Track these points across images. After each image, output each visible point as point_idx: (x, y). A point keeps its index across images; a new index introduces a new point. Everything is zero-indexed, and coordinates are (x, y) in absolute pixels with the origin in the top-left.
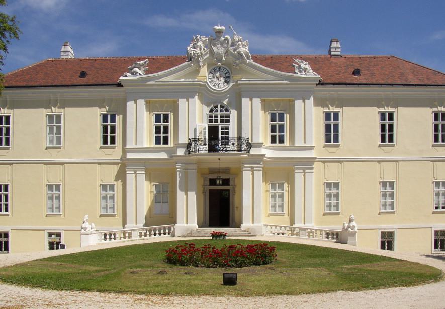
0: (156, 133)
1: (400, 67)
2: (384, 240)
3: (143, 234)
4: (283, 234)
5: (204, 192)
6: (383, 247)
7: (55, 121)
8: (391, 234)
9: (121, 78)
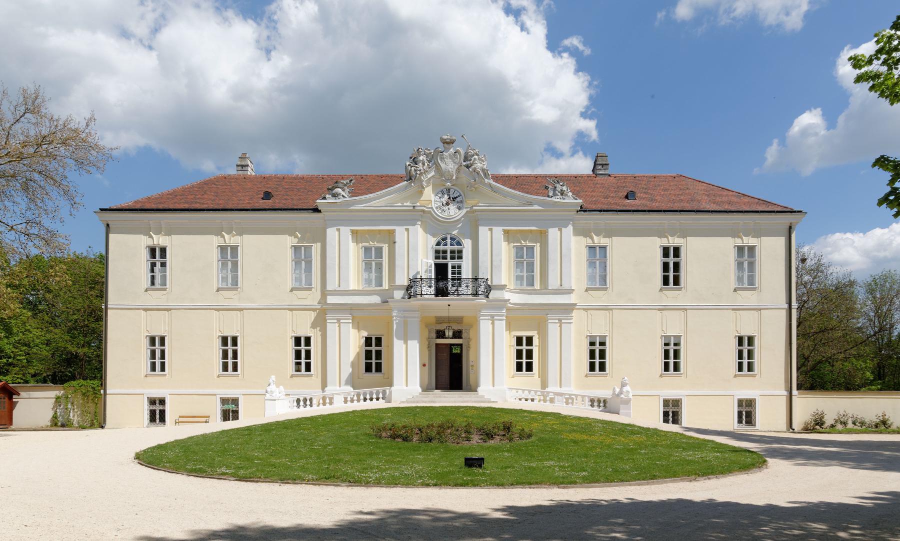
5: (429, 346)
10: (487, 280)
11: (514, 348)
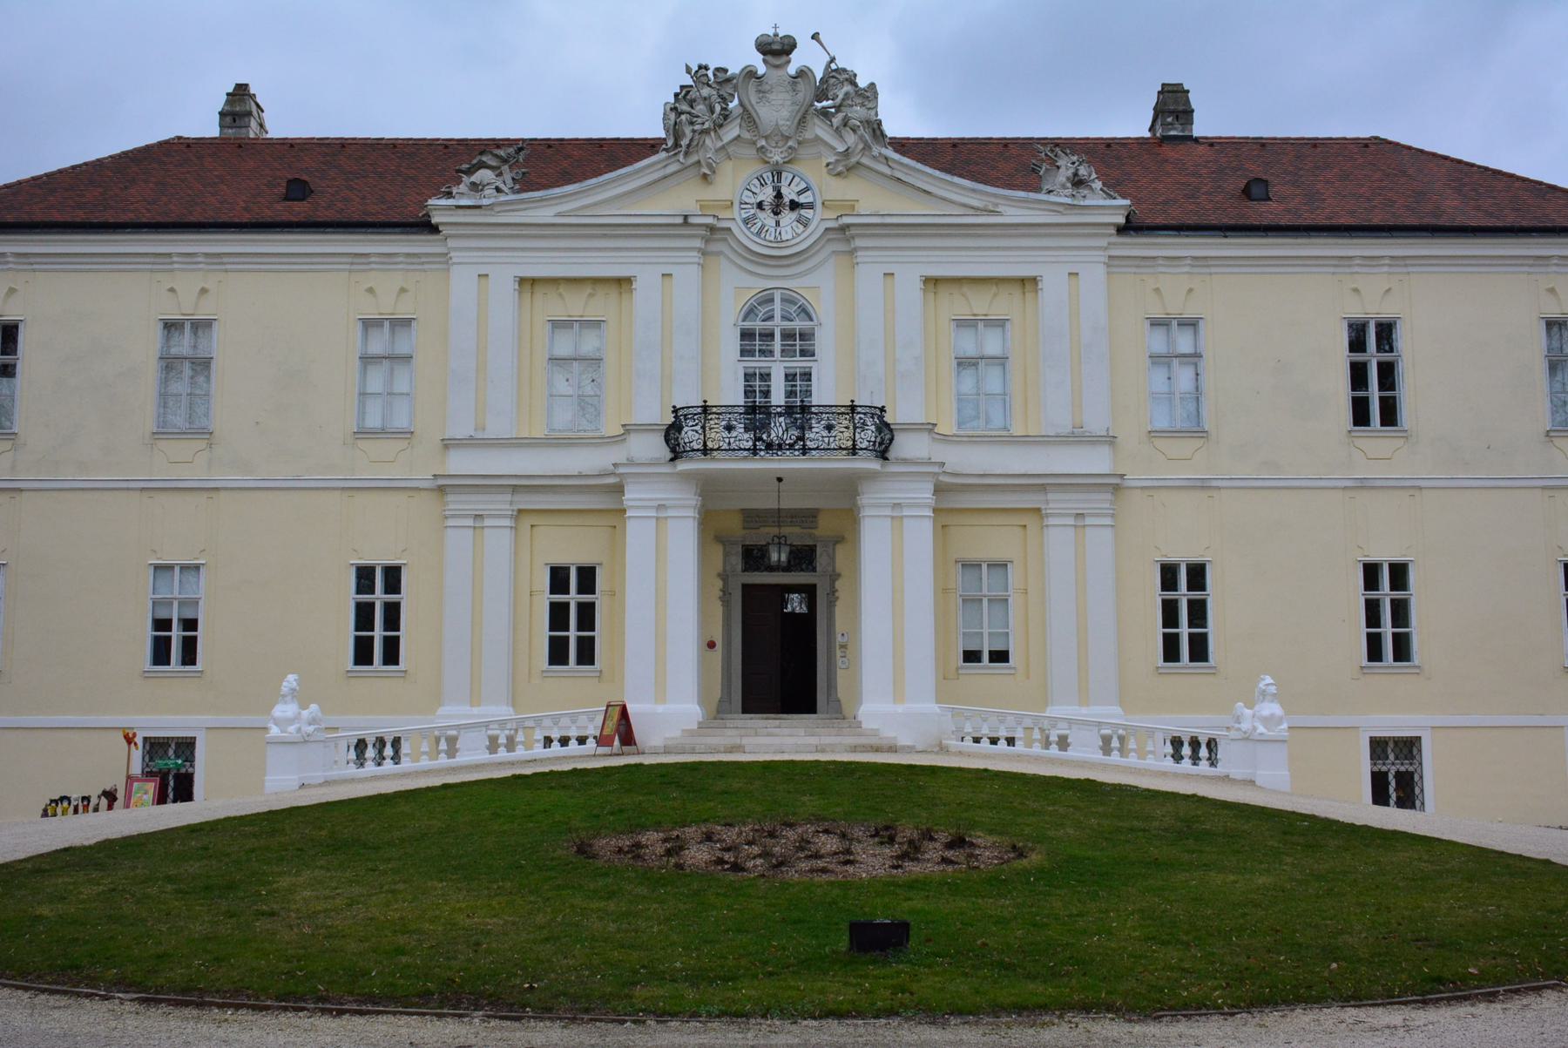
0: (1204, 637)
1: (1411, 172)
2: (1384, 769)
3: (502, 740)
4: (1011, 741)
6: (1380, 797)
7: (392, 370)
8: (1408, 747)
9: (430, 202)
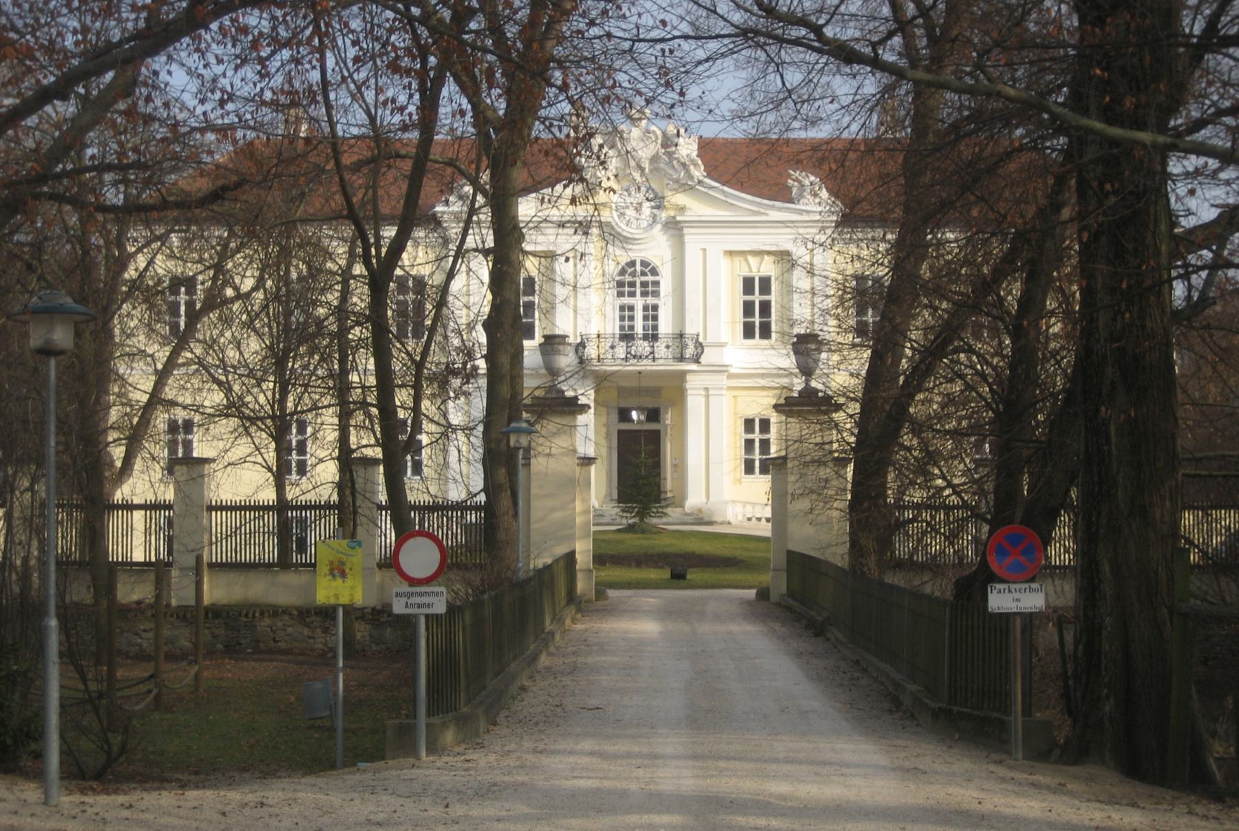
5: (608, 435)
10: (698, 335)
11: (740, 298)
